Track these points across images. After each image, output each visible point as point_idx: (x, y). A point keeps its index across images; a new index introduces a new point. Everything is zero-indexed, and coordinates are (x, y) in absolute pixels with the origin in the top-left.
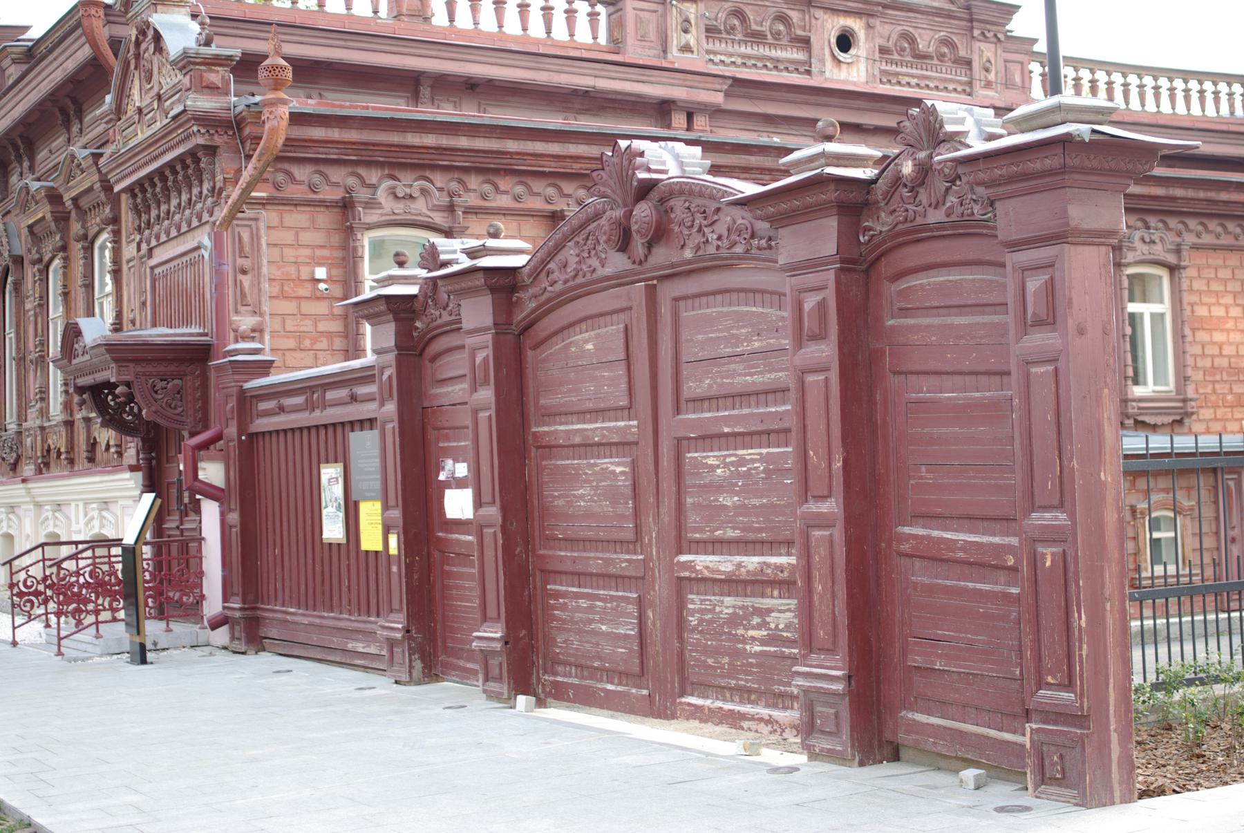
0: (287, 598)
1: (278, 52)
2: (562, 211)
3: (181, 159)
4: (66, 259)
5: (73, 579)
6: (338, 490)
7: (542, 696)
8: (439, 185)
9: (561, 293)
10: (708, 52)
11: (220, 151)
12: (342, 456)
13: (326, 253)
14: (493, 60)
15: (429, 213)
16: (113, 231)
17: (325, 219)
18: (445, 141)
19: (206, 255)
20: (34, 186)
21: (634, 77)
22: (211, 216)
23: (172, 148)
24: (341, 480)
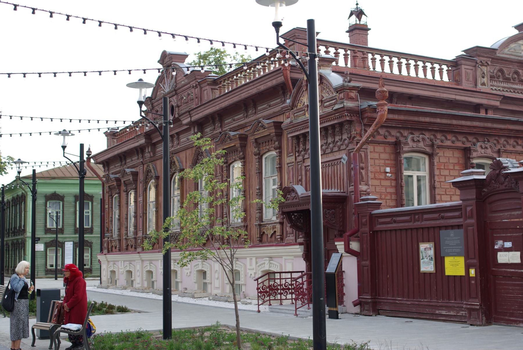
2: (470, 147)
5: (301, 286)
10: (491, 85)
13: (389, 162)
14: (423, 88)
15: (425, 147)
18: (433, 120)
21: (469, 95)
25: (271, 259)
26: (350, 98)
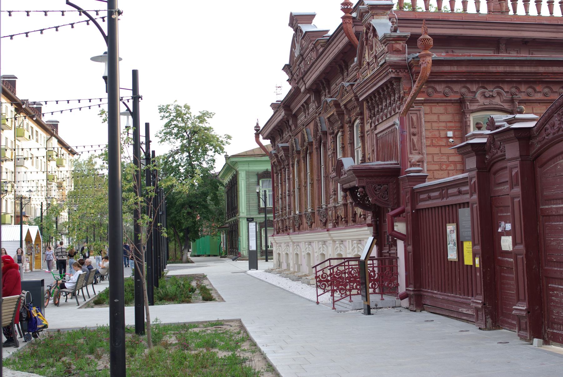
0: (433, 286)
1: (426, 33)
3: (385, 84)
4: (343, 132)
6: (454, 236)
7: (547, 339)
8: (506, 90)
9: (553, 139)
11: (402, 79)
12: (455, 220)
15: (502, 104)
16: (361, 118)
17: (451, 109)
18: (508, 69)
19: (397, 127)
20: (329, 100)
22: (399, 109)
23: (381, 80)
24: (455, 231)
25: (359, 242)
26: (395, 51)
